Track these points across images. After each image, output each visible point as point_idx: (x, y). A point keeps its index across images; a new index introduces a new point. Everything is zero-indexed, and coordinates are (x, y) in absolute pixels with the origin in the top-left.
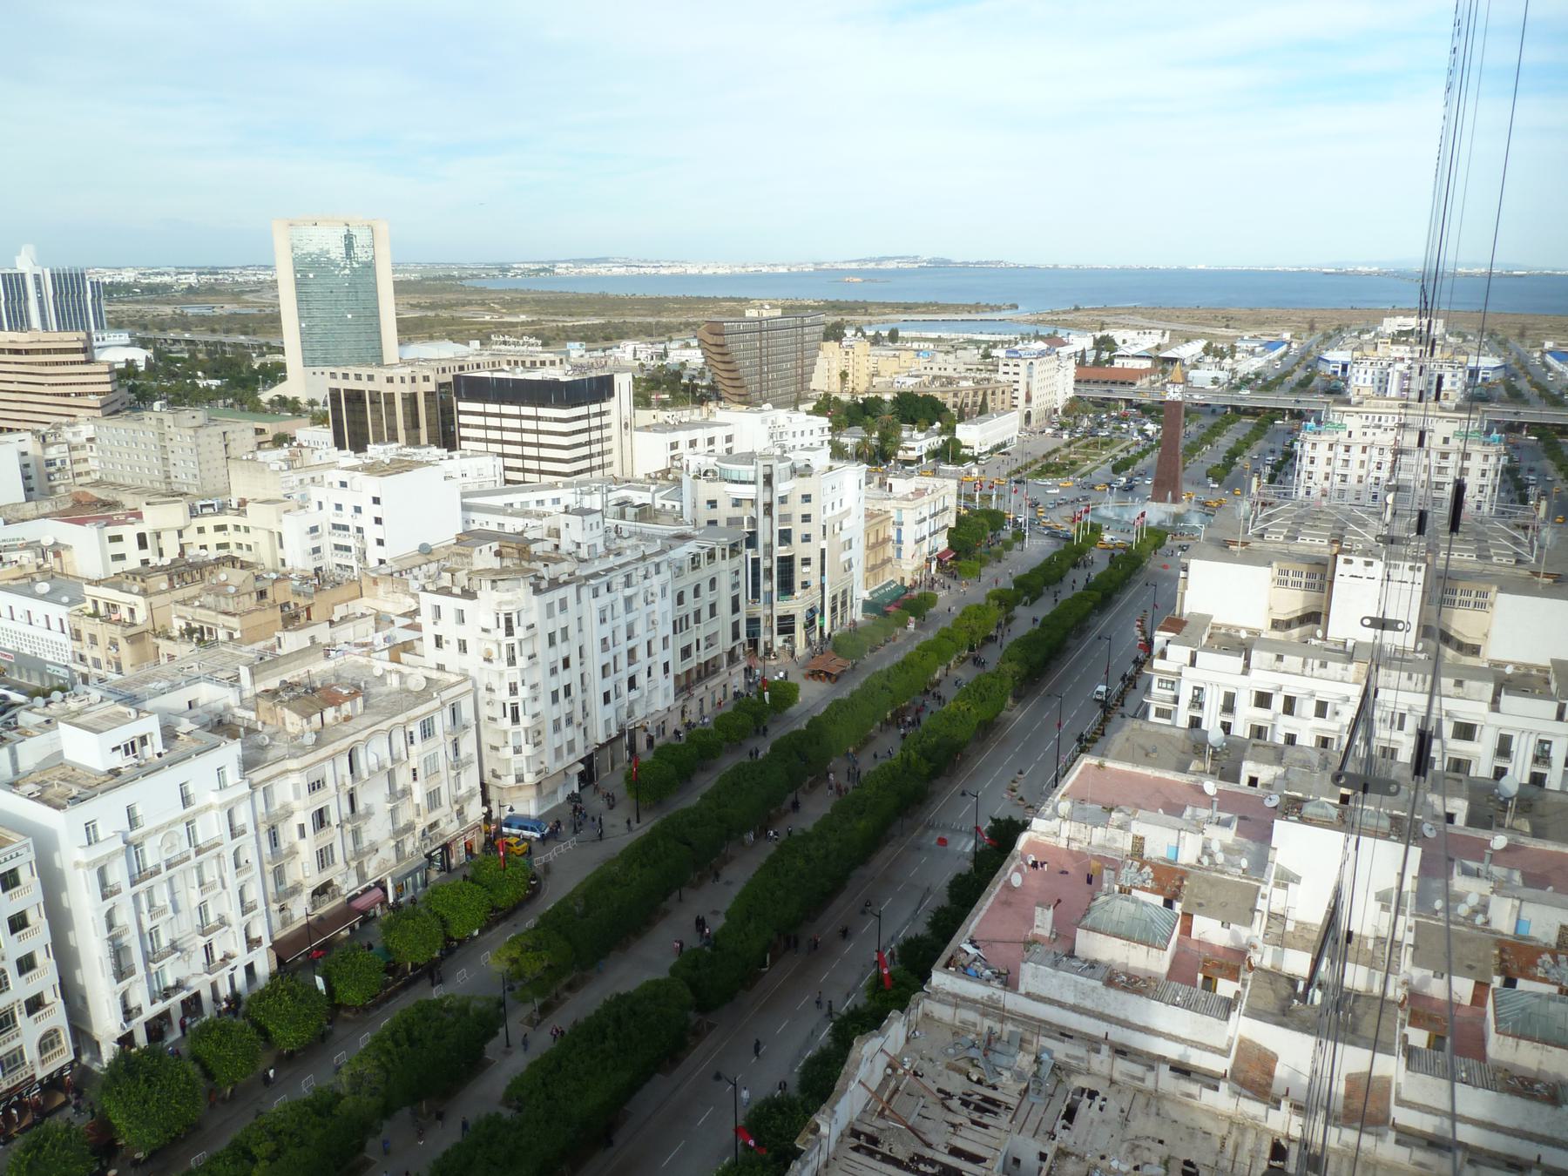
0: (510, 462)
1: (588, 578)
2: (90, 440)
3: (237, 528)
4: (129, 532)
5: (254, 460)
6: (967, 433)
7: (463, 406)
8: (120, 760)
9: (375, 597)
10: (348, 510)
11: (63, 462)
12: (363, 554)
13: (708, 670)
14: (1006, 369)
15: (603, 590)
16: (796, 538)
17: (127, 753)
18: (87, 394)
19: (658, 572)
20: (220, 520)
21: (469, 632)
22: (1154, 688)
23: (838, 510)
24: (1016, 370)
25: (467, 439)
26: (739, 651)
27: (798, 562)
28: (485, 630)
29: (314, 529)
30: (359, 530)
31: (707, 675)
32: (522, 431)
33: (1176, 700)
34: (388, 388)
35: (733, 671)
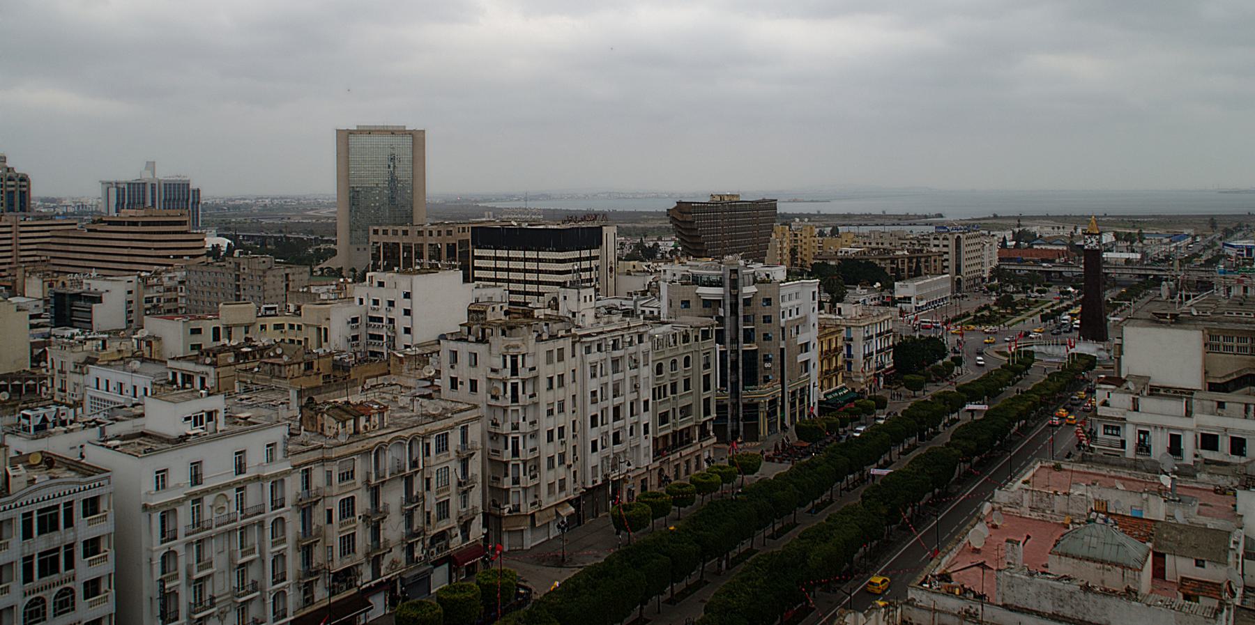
0: (513, 287)
1: (581, 336)
2: (181, 282)
3: (292, 326)
4: (208, 326)
5: (309, 292)
6: (900, 290)
7: (477, 252)
8: (188, 428)
9: (400, 374)
10: (383, 305)
11: (159, 300)
12: (392, 340)
13: (681, 439)
14: (936, 242)
15: (594, 349)
16: (758, 337)
17: (196, 425)
18: (182, 257)
19: (640, 341)
20: (278, 320)
21: (481, 374)
22: (1100, 434)
23: (794, 316)
24: (945, 243)
25: (480, 268)
26: (710, 427)
27: (760, 357)
28: (493, 370)
29: (355, 320)
30: (391, 321)
31: (681, 444)
32: (526, 282)
33: (1123, 444)
34: (419, 240)
35: (704, 444)
